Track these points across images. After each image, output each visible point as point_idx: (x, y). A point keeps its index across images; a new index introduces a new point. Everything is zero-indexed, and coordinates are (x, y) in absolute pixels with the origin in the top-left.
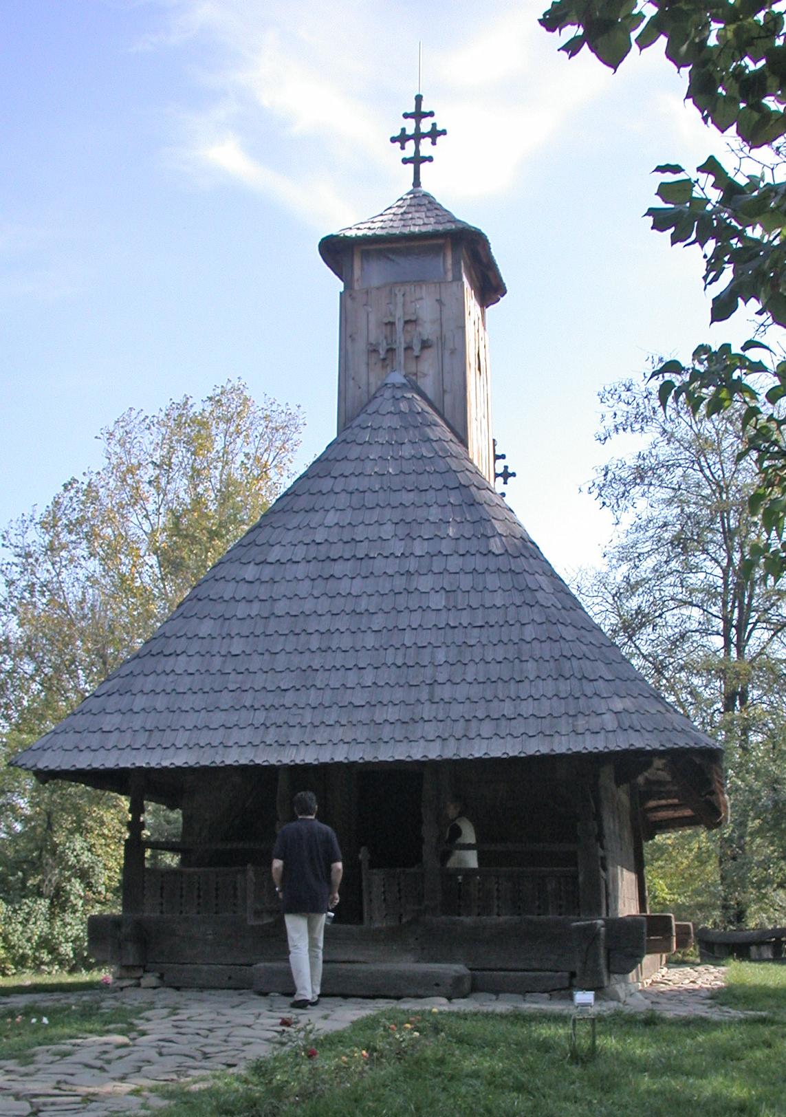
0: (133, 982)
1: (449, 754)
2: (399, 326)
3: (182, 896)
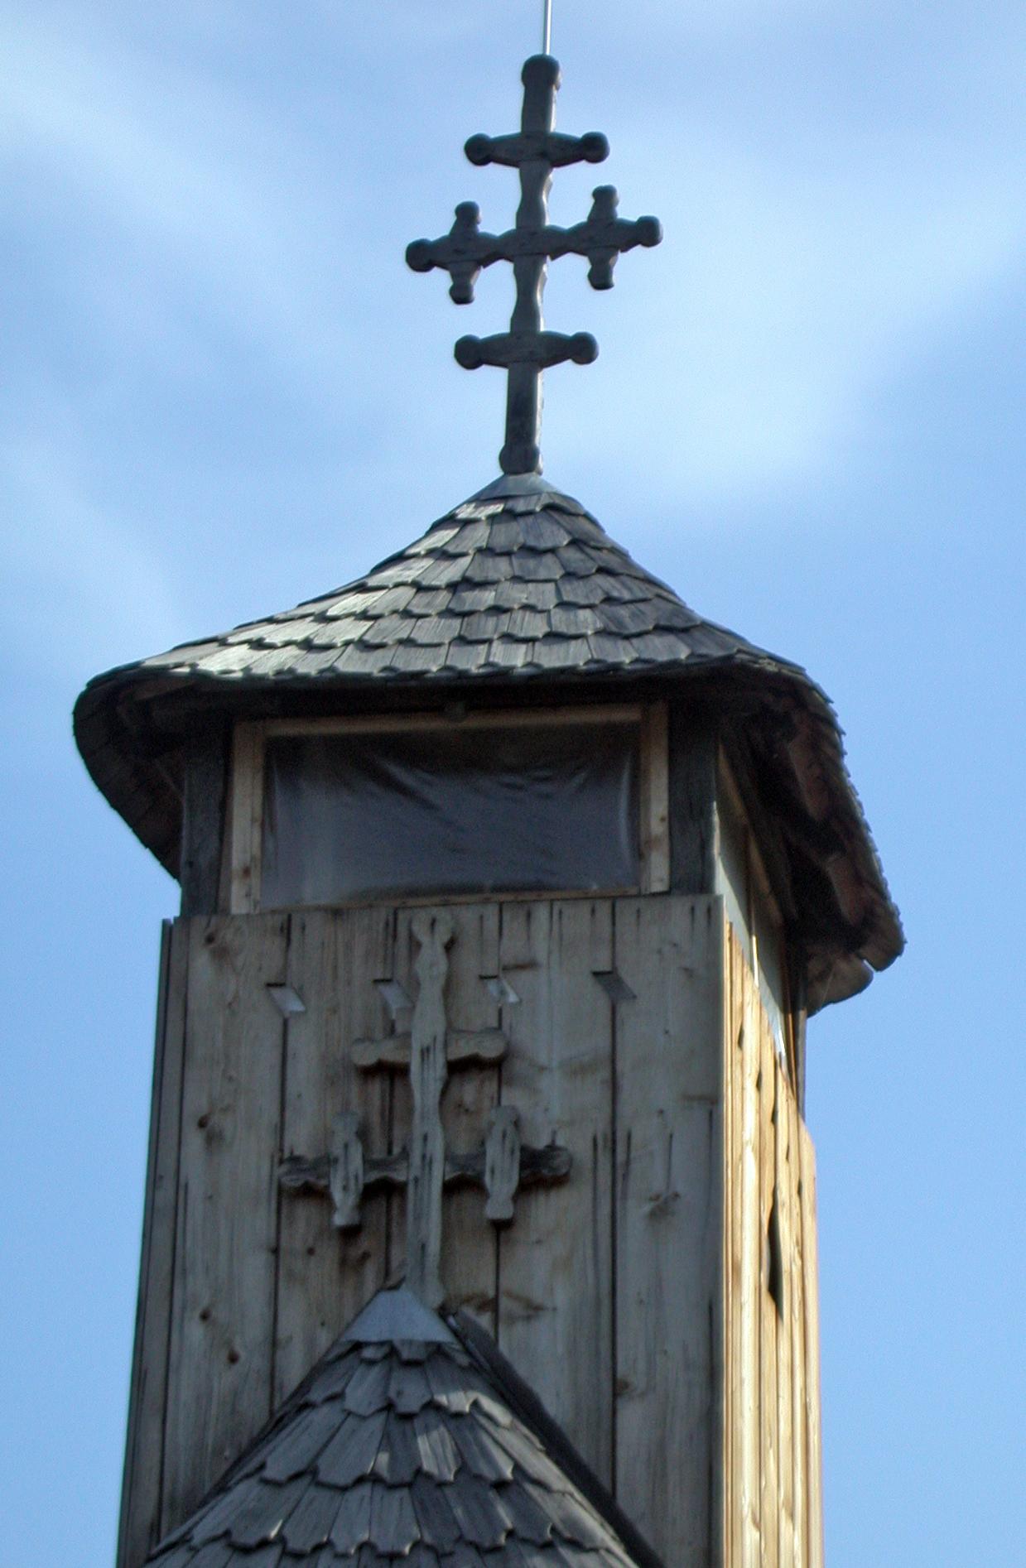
2: (426, 1082)
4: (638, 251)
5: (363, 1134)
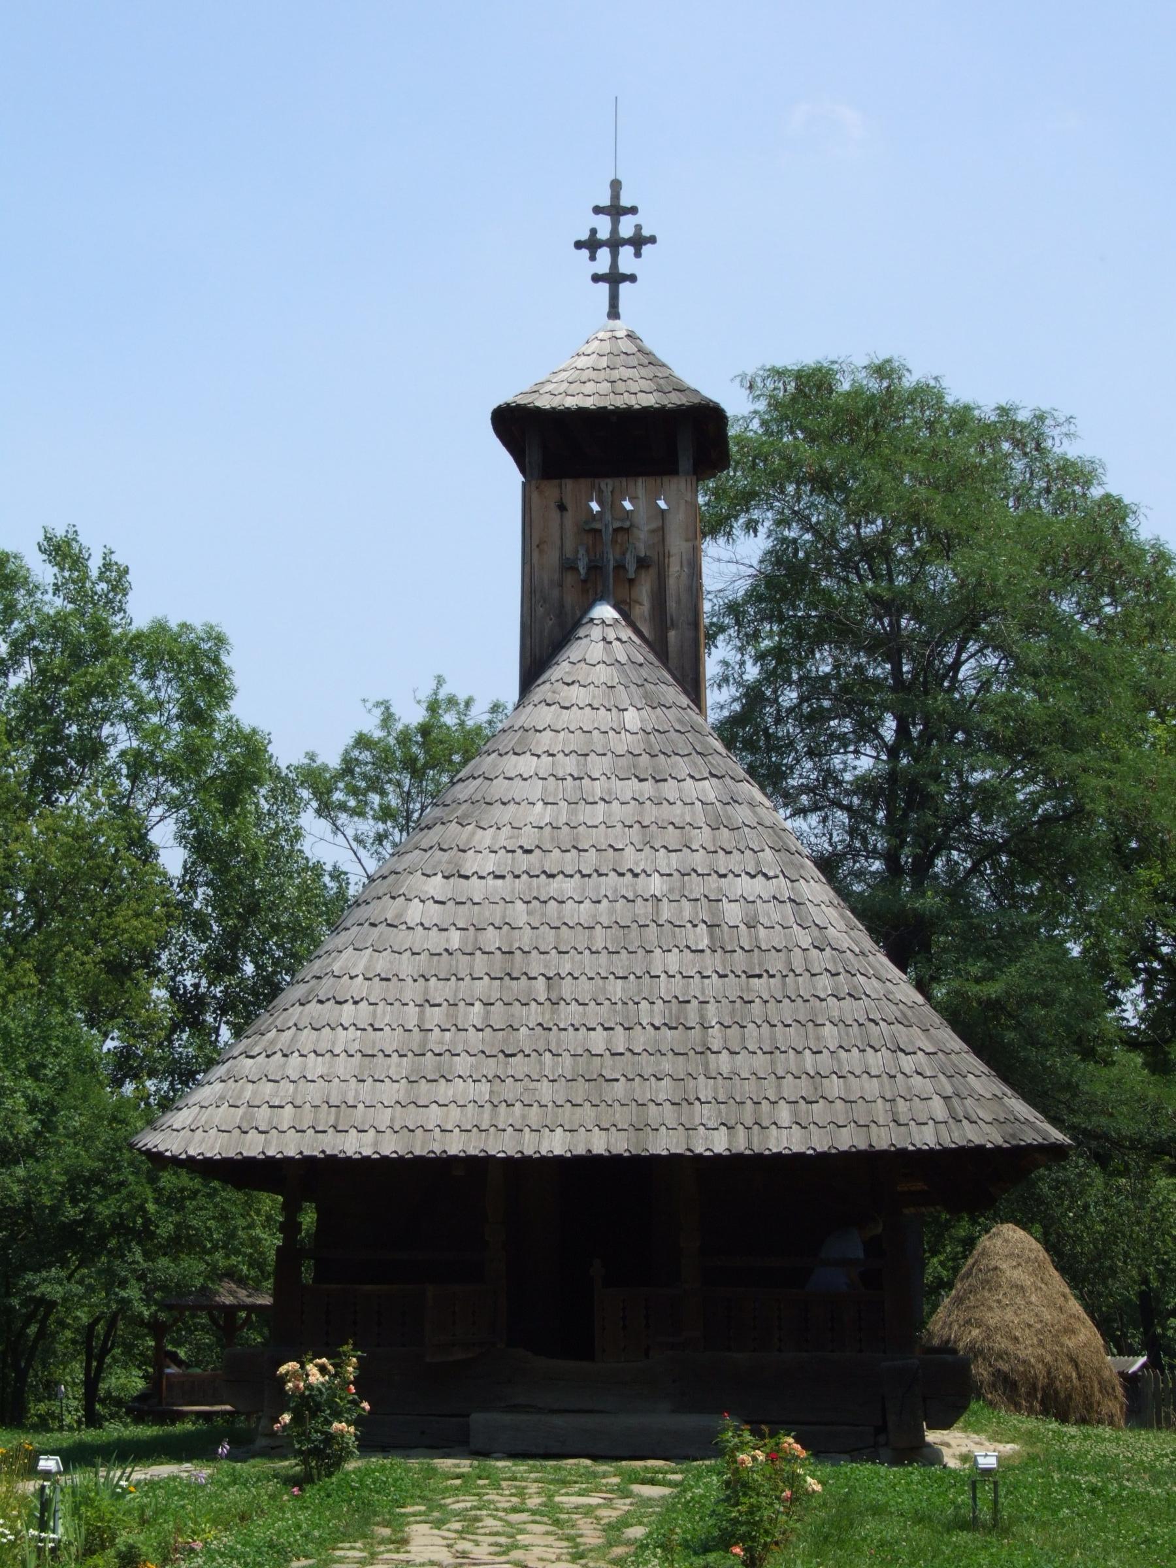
1: (741, 1145)
2: (607, 536)
4: (649, 245)
5: (587, 551)
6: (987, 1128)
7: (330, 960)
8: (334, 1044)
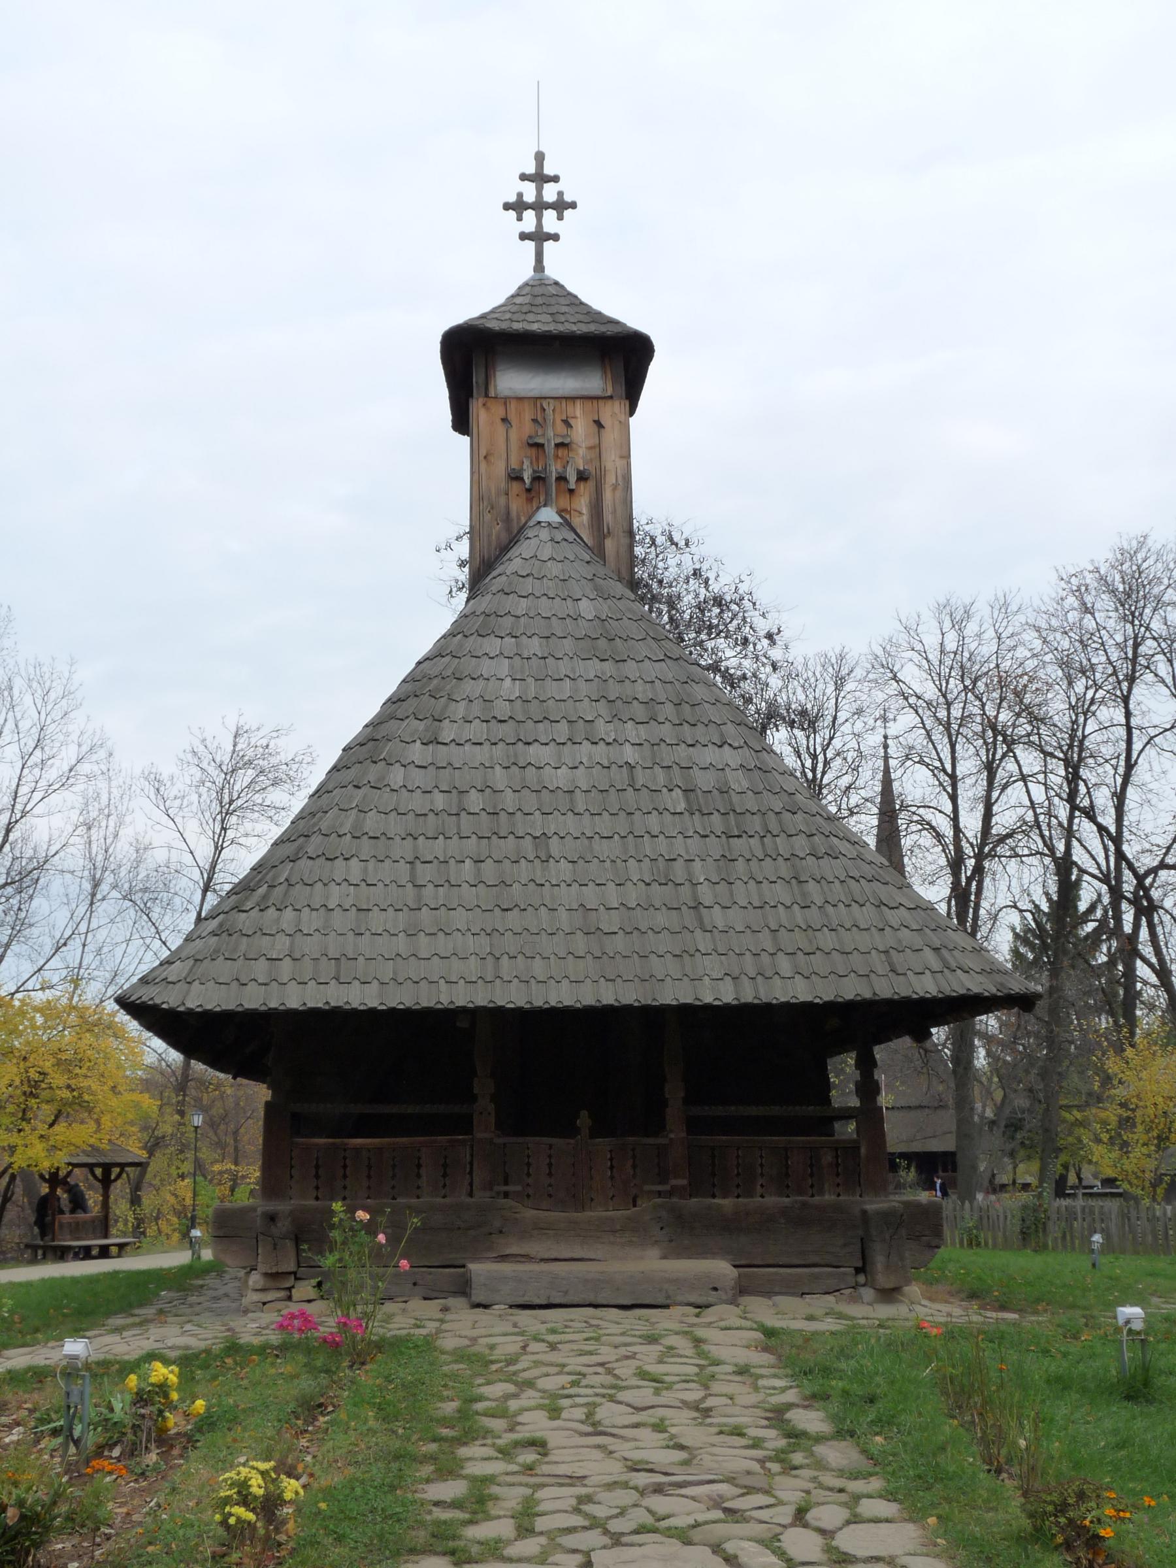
0: (282, 1294)
2: (550, 449)
3: (345, 1176)
6: (980, 978)
7: (315, 820)
8: (327, 898)
